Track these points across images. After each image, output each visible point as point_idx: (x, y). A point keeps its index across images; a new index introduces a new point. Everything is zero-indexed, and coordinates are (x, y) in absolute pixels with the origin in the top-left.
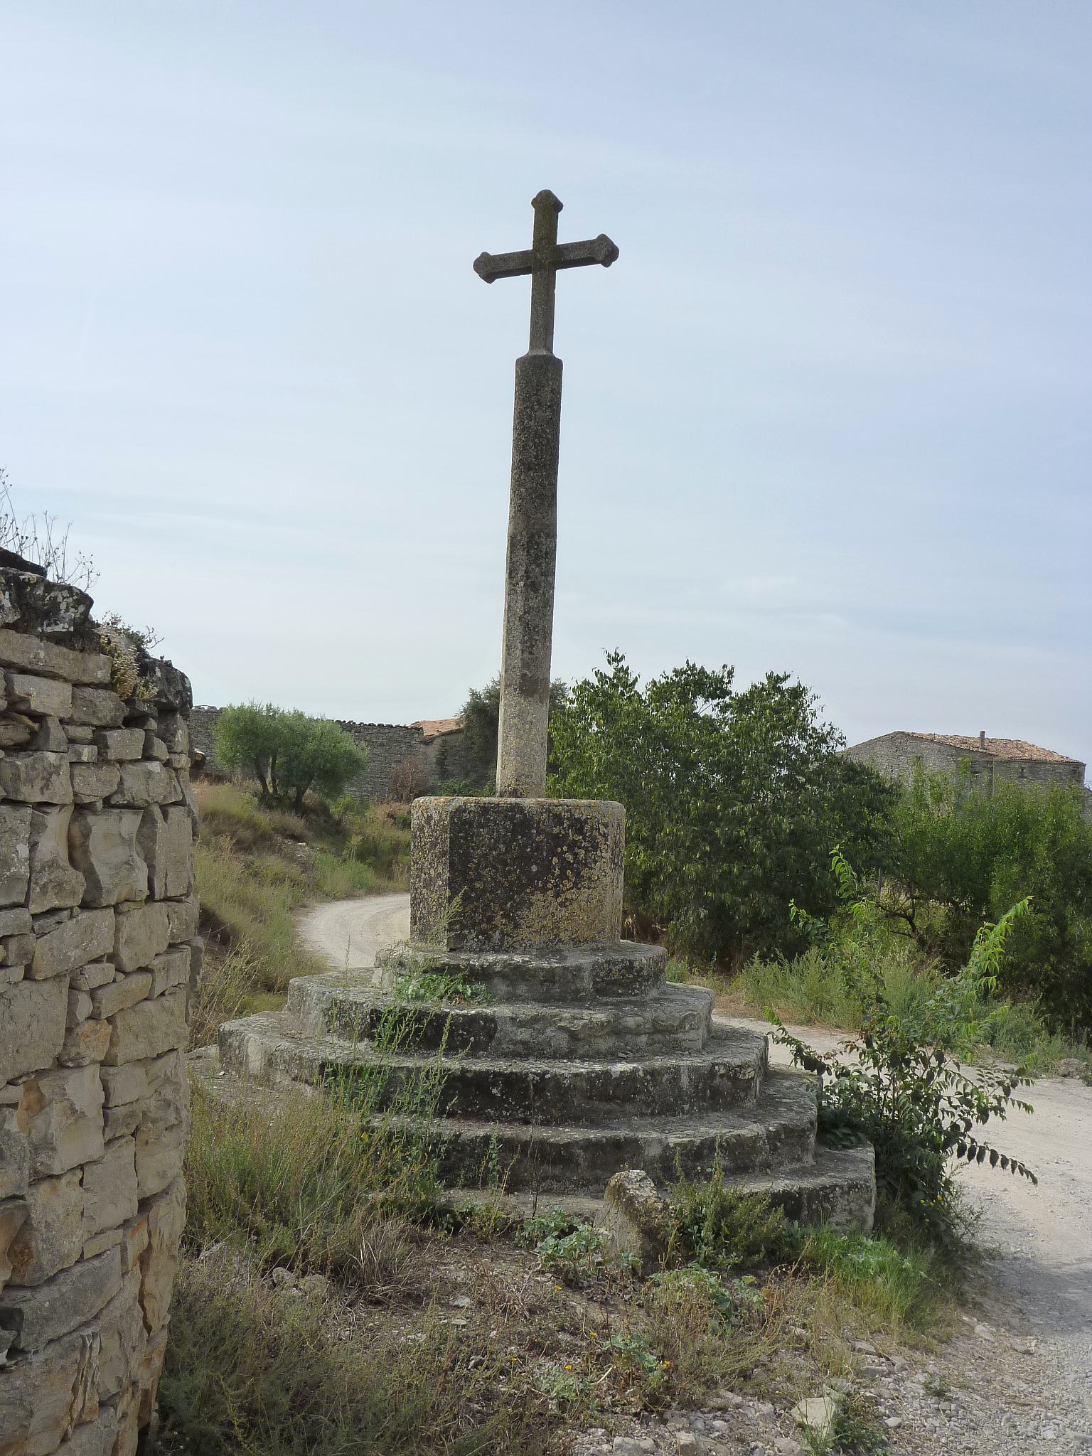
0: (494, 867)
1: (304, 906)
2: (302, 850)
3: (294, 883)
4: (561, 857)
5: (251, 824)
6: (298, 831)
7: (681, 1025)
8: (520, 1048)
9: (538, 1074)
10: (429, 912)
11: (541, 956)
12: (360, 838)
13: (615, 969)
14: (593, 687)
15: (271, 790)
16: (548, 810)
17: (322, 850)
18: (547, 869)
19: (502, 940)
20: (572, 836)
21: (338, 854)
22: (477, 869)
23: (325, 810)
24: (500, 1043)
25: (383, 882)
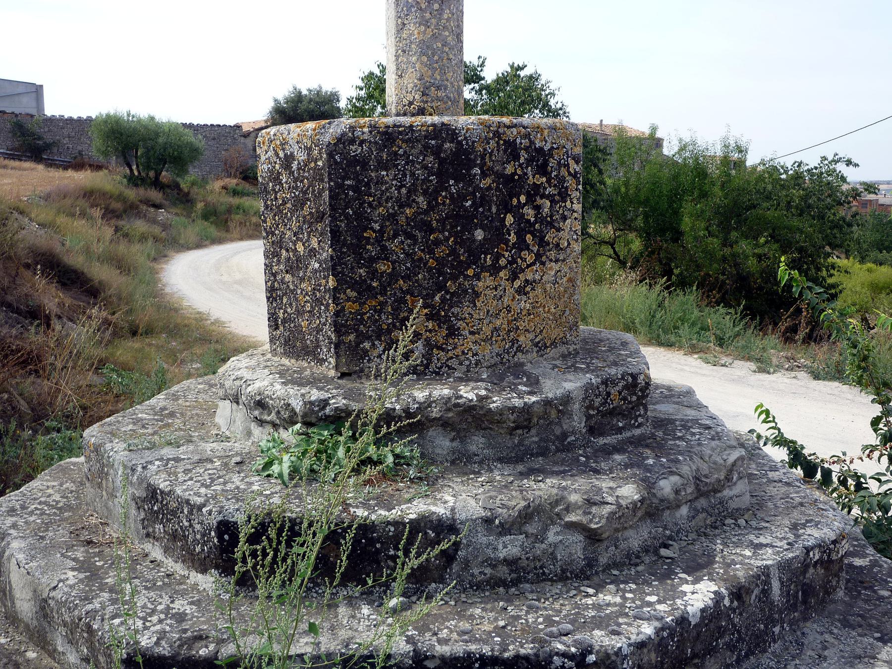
0: (409, 236)
1: (165, 256)
2: (162, 215)
3: (156, 239)
4: (517, 211)
5: (120, 198)
6: (158, 202)
7: (728, 478)
8: (503, 572)
9: (571, 657)
10: (300, 313)
11: (497, 381)
12: (202, 204)
13: (614, 391)
14: (377, 76)
15: (136, 173)
16: (497, 134)
17: (176, 214)
18: (497, 235)
19: (428, 356)
20: (534, 179)
21: (188, 216)
22: (378, 241)
23: (177, 186)
24: (467, 564)
25: (223, 234)
